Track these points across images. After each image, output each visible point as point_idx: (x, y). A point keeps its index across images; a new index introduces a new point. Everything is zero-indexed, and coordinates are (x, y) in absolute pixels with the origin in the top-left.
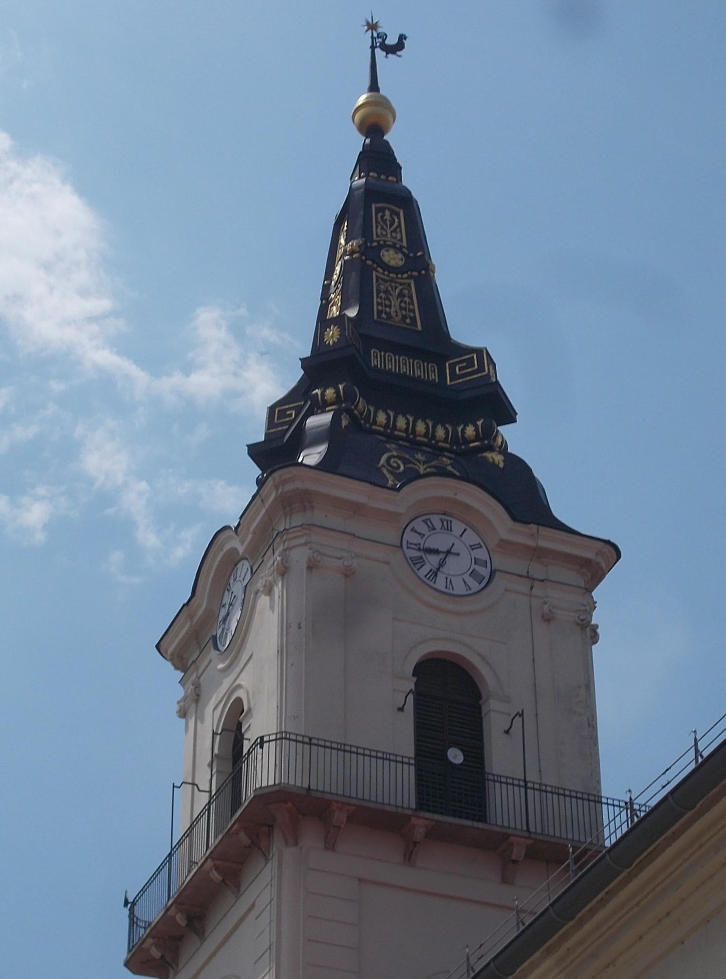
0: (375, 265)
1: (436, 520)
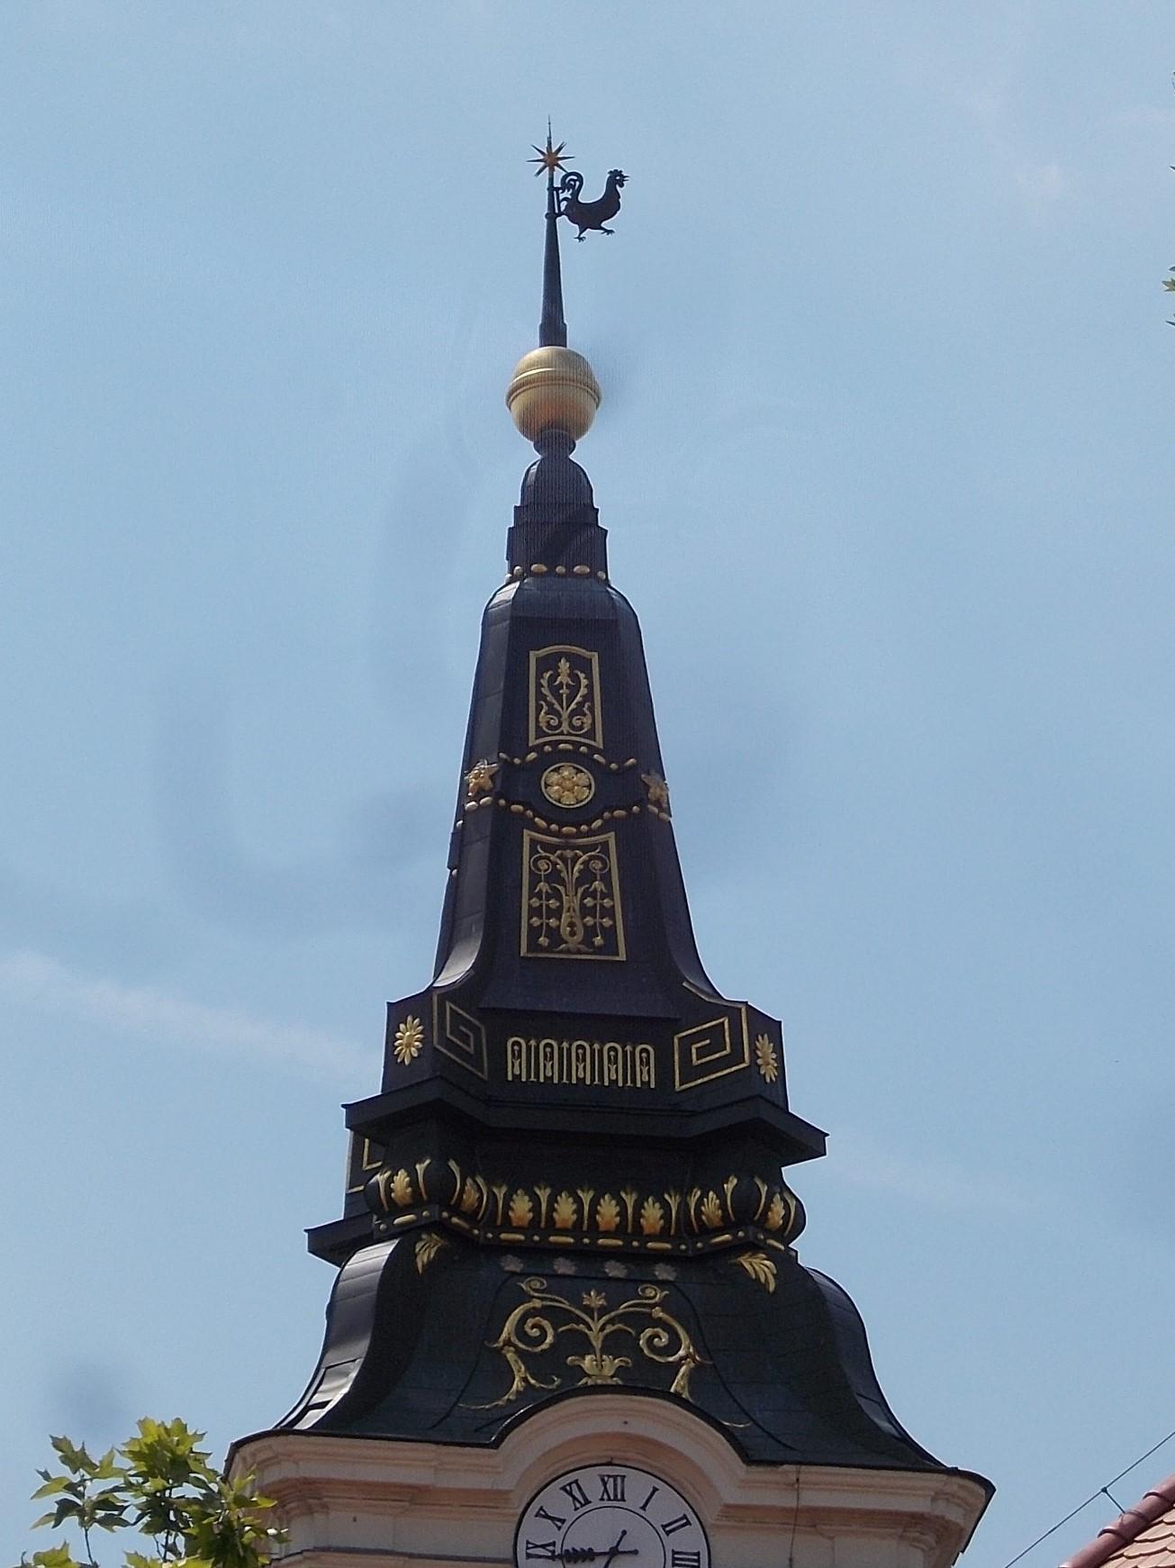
0: (529, 813)
1: (590, 1482)
